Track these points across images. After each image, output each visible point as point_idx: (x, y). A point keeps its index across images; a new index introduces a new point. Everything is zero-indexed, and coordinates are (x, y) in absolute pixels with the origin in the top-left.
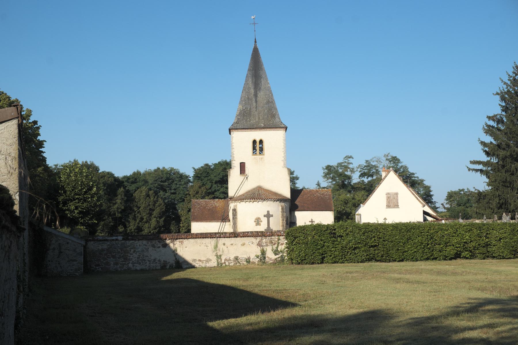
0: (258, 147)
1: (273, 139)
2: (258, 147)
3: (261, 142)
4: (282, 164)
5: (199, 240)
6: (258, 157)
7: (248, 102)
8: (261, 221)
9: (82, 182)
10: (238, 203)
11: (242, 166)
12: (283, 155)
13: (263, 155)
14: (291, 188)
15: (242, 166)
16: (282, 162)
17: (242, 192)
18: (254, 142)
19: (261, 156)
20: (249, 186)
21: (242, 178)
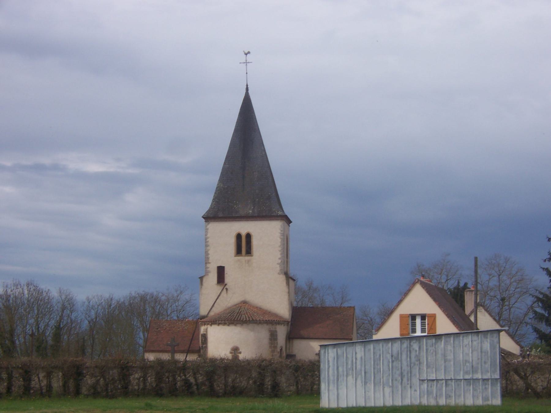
0: (244, 245)
1: (266, 234)
2: (244, 245)
3: (249, 236)
4: (278, 268)
5: (478, 319)
6: (244, 259)
7: (524, 378)
8: (240, 353)
9: (32, 294)
10: (209, 326)
11: (221, 271)
12: (280, 256)
13: (252, 256)
14: (291, 304)
15: (221, 271)
16: (278, 266)
17: (218, 309)
18: (239, 236)
19: (247, 258)
20: (230, 300)
21: (220, 288)
